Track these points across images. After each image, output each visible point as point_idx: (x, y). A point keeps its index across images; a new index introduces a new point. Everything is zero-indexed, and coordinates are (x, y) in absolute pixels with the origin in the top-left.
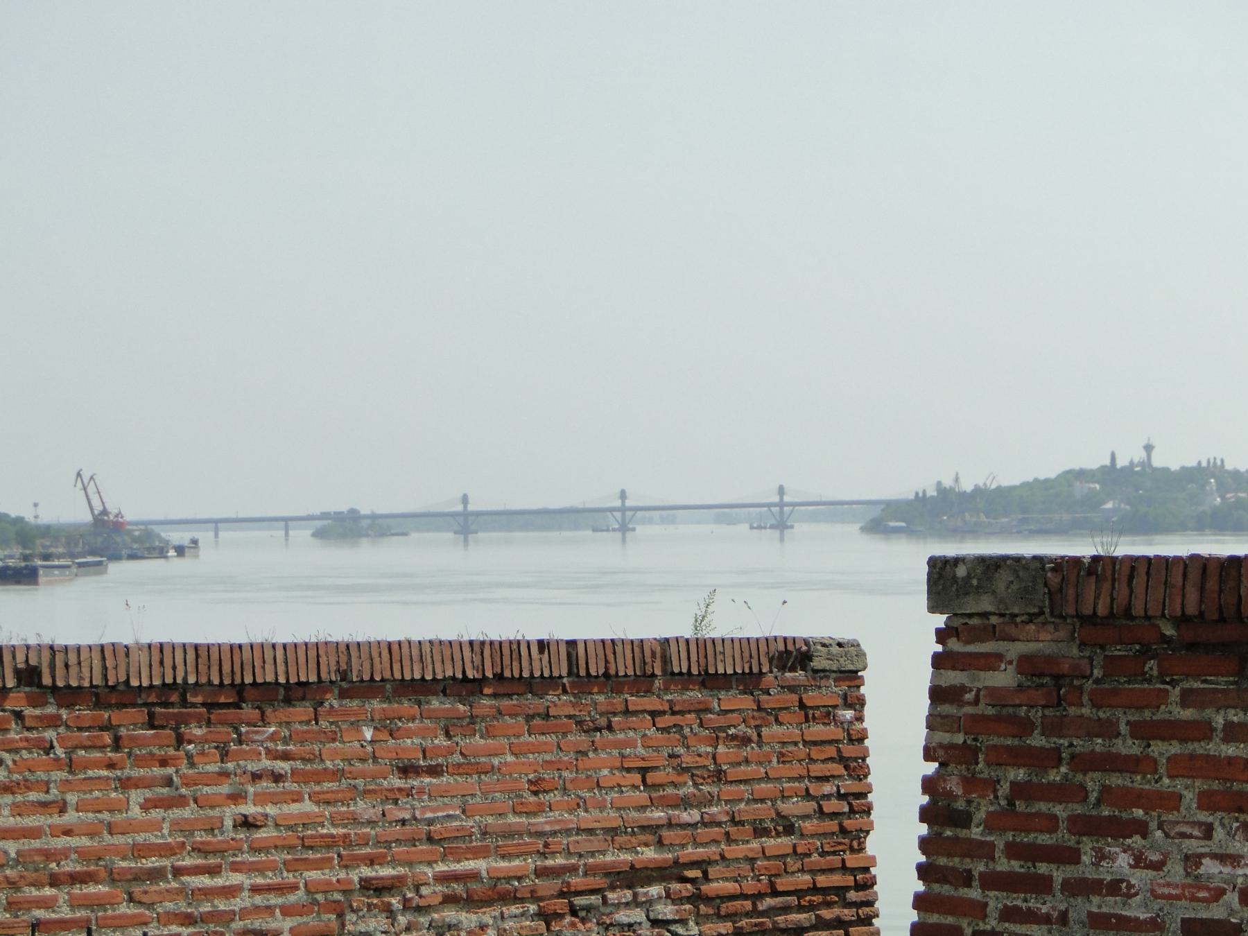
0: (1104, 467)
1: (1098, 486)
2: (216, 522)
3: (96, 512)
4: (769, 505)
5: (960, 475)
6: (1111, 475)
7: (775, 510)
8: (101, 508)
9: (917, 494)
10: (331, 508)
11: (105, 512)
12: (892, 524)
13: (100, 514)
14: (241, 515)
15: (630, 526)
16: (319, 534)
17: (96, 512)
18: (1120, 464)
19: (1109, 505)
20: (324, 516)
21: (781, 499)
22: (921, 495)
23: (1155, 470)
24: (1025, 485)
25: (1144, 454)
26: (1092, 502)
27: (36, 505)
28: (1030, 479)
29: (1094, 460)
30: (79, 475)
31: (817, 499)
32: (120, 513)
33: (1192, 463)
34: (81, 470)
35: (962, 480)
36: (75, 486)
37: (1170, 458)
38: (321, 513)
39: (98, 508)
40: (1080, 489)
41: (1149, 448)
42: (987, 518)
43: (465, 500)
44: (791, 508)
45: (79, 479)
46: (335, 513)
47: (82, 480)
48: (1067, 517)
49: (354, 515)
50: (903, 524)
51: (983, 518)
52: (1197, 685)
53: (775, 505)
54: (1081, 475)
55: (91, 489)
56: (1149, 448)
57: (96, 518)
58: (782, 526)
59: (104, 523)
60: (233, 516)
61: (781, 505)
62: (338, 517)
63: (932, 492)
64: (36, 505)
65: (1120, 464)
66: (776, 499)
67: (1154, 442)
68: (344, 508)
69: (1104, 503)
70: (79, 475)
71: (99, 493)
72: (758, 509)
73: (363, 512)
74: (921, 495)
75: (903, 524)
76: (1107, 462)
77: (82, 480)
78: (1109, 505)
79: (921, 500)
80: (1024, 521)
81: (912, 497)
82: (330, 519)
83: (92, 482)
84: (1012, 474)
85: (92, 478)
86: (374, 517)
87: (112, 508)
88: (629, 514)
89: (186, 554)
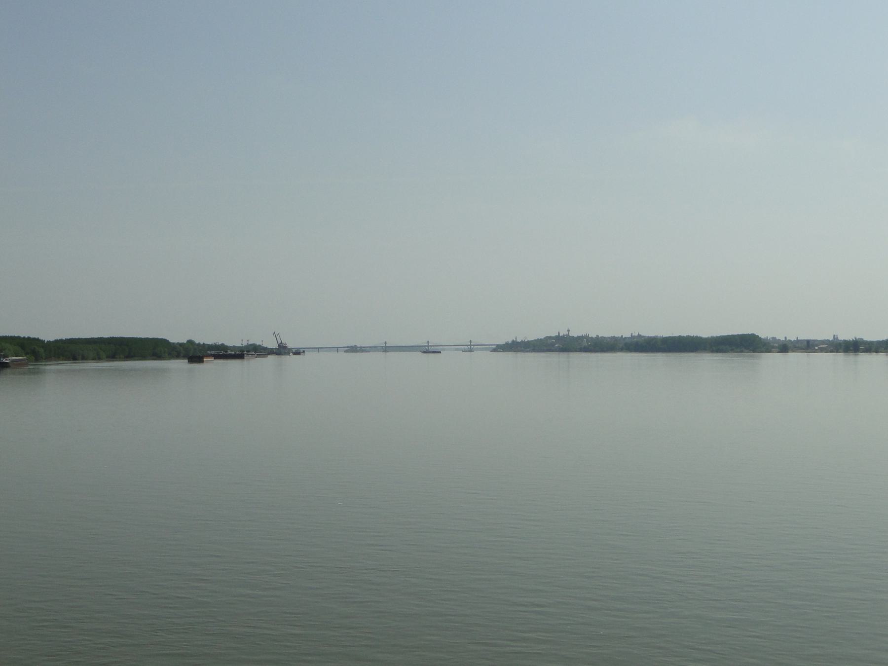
0: (795, 340)
1: (554, 341)
2: (319, 348)
4: (383, 347)
6: (558, 338)
7: (469, 347)
8: (280, 342)
11: (281, 343)
16: (346, 351)
18: (561, 335)
19: (557, 346)
20: (348, 347)
23: (570, 336)
24: (535, 340)
25: (567, 333)
26: (553, 345)
27: (242, 340)
28: (536, 339)
29: (554, 334)
30: (274, 333)
33: (580, 335)
35: (517, 339)
37: (574, 333)
39: (279, 342)
40: (549, 341)
41: (569, 331)
43: (386, 343)
48: (545, 348)
51: (523, 348)
52: (617, 658)
53: (426, 346)
54: (550, 338)
55: (278, 337)
56: (569, 331)
57: (279, 346)
58: (471, 350)
61: (471, 345)
63: (851, 340)
64: (242, 340)
65: (561, 335)
67: (570, 329)
68: (354, 345)
69: (555, 345)
70: (274, 333)
72: (441, 347)
73: (358, 346)
76: (796, 339)
78: (557, 346)
79: (507, 344)
81: (505, 343)
84: (531, 337)
86: (361, 347)
88: (472, 347)
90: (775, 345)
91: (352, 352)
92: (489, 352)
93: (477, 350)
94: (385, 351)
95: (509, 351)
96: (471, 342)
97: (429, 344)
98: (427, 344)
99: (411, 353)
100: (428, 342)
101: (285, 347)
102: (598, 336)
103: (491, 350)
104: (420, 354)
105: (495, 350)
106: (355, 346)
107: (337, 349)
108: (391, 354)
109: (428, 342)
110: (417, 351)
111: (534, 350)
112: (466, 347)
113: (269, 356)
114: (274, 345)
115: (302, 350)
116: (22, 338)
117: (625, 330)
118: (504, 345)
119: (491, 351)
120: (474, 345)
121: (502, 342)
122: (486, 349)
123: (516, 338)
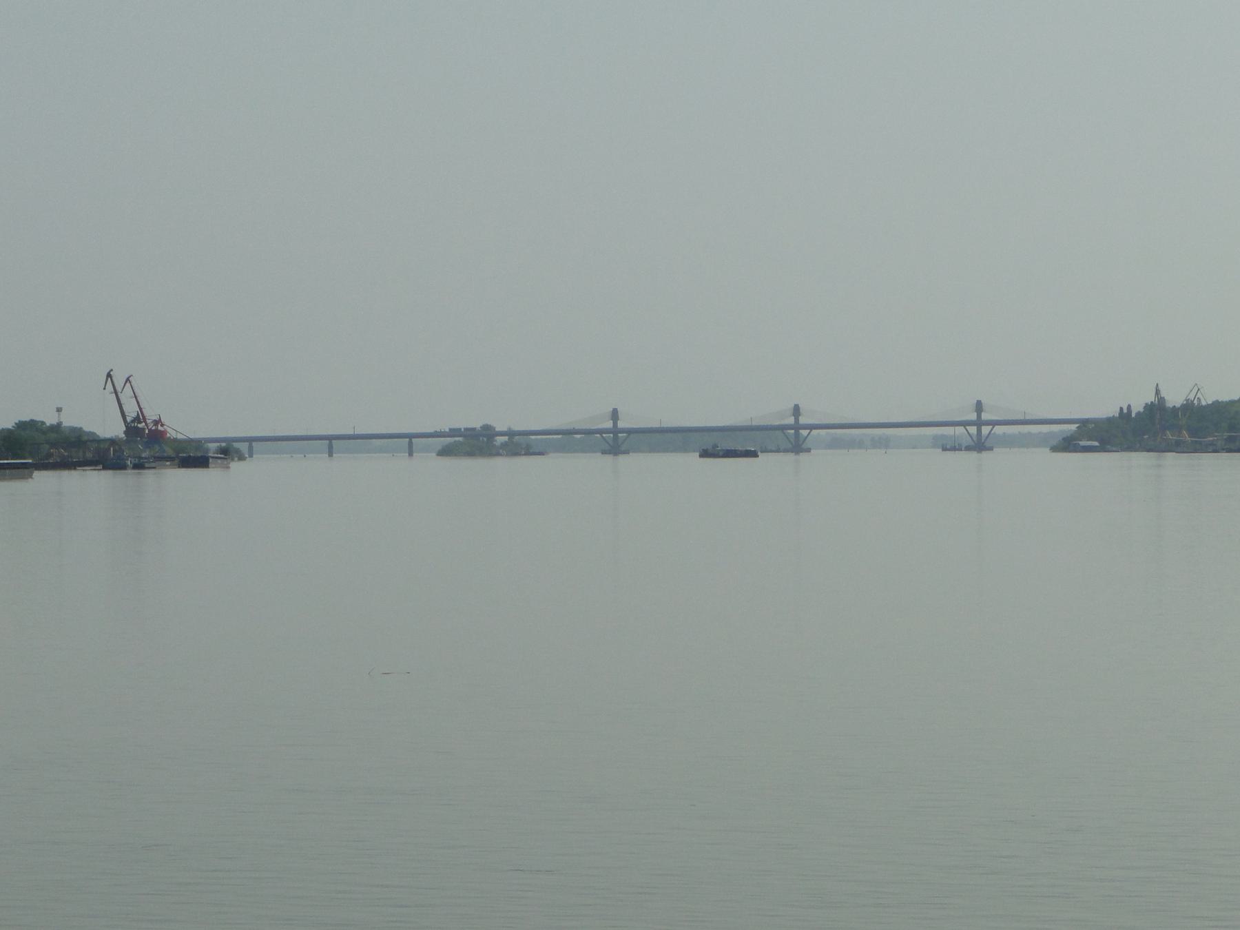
2: (330, 438)
3: (129, 419)
4: (601, 432)
5: (1160, 387)
7: (973, 430)
8: (134, 415)
9: (1121, 409)
10: (462, 424)
12: (1083, 443)
13: (133, 421)
14: (359, 431)
15: (804, 446)
16: (445, 452)
17: (129, 419)
20: (454, 432)
21: (979, 416)
22: (1125, 411)
27: (59, 410)
30: (109, 375)
31: (1020, 417)
32: (160, 419)
34: (112, 370)
36: (104, 389)
38: (450, 429)
39: (131, 411)
42: (1172, 436)
43: (615, 415)
44: (808, 431)
45: (109, 379)
46: (466, 429)
47: (112, 380)
49: (488, 432)
50: (1096, 444)
51: (1186, 436)
55: (126, 396)
58: (980, 446)
59: (139, 432)
60: (351, 432)
61: (979, 423)
62: (470, 434)
64: (59, 410)
66: (973, 416)
68: (477, 424)
70: (109, 375)
71: (136, 397)
73: (499, 427)
74: (1125, 411)
75: (1096, 444)
77: (112, 380)
80: (1231, 439)
82: (460, 436)
83: (128, 384)
85: (128, 380)
86: (511, 434)
87: (151, 415)
88: (804, 433)
89: (210, 465)
90: (141, 448)
91: (471, 454)
92: (1044, 455)
93: (1009, 442)
94: (615, 449)
95: (1130, 448)
96: (979, 407)
97: (802, 420)
98: (973, 416)
99: (1006, 418)
100: (796, 411)
101: (156, 436)
102: (1174, 406)
103: (1054, 442)
104: (693, 458)
105: (1068, 445)
106: (487, 428)
107: (410, 442)
108: (632, 463)
109: (796, 411)
110: (684, 448)
111: (121, 412)
112: (960, 430)
113: (36, 474)
114: (110, 427)
115: (244, 447)
116: (29, 422)
117: (431, 430)
118: (1110, 420)
119: (1055, 449)
120: (994, 423)
121: (1104, 408)
122: (1040, 441)
123: (1157, 392)
